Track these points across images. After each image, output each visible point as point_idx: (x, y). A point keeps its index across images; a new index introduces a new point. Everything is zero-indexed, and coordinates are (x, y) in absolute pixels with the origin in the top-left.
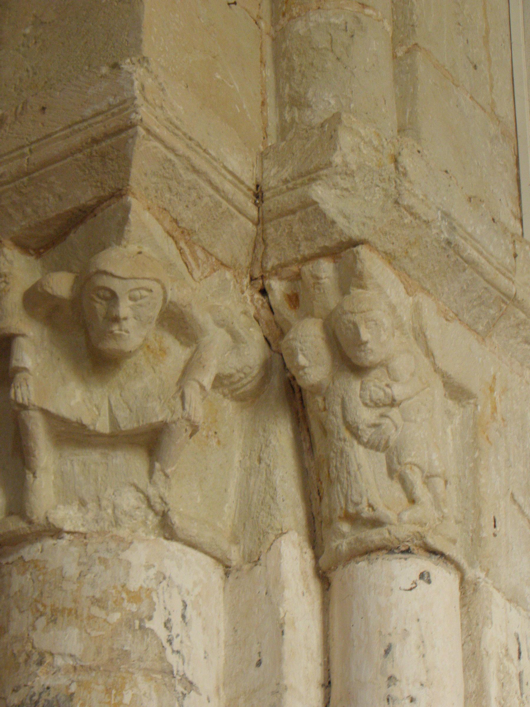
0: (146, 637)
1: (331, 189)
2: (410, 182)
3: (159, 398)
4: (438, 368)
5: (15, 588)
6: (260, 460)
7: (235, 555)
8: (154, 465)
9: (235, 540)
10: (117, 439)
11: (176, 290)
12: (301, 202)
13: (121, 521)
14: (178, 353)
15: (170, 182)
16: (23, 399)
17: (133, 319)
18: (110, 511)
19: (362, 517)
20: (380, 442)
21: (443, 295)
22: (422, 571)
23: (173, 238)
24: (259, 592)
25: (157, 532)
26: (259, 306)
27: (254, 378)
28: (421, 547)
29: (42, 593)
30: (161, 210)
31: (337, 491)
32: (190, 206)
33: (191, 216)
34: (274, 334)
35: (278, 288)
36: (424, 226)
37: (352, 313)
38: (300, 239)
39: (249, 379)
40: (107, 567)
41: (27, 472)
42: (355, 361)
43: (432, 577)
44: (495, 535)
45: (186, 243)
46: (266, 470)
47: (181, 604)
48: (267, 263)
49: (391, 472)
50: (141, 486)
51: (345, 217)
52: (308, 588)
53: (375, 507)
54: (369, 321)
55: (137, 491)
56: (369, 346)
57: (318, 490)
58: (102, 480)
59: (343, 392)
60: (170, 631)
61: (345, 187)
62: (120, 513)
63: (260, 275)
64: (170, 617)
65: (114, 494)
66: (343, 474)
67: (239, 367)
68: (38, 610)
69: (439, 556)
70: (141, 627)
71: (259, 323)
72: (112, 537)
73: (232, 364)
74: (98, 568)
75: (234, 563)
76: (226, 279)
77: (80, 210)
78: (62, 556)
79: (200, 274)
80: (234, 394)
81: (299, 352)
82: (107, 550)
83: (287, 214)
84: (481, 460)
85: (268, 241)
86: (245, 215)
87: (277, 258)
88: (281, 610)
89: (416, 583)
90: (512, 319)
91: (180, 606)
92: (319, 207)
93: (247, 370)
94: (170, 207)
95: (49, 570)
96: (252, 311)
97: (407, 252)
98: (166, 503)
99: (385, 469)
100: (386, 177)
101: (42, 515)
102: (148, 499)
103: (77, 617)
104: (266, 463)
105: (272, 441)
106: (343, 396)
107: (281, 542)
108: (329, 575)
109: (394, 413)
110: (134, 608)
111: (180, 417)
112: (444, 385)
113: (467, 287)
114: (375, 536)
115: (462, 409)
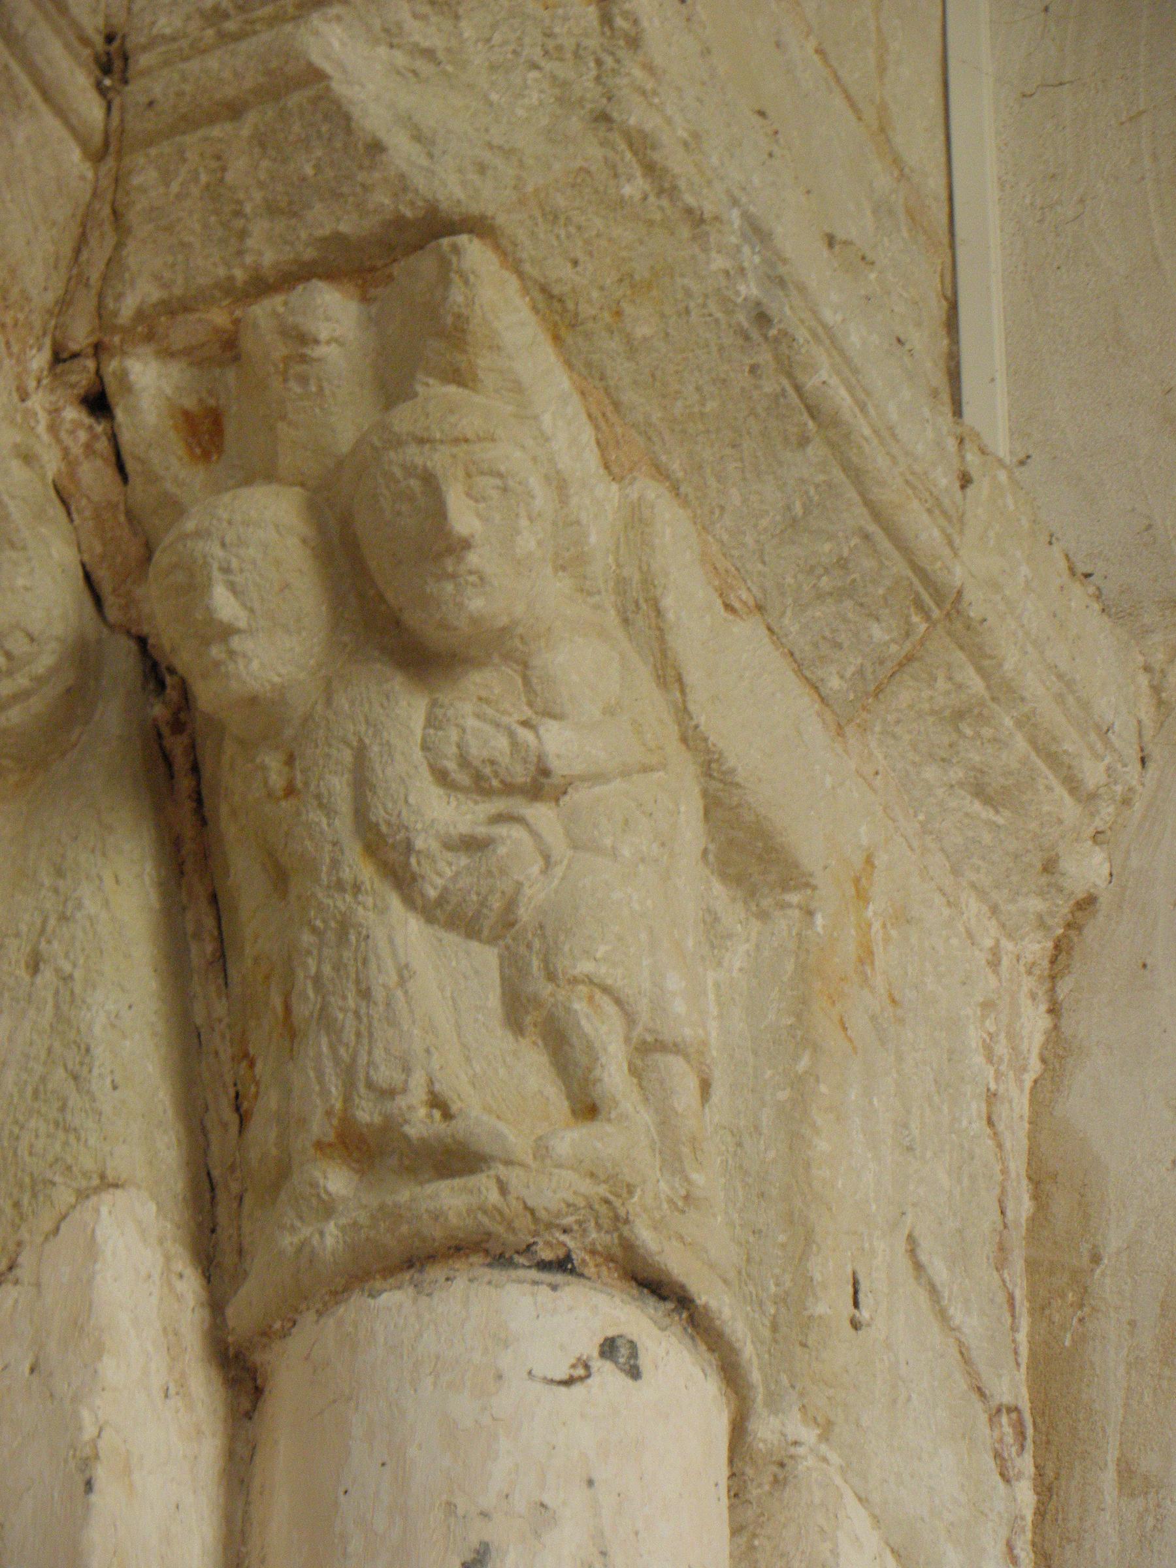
1: (377, 42)
2: (649, 68)
4: (696, 727)
6: (35, 964)
12: (269, 73)
19: (405, 1137)
20: (483, 903)
21: (721, 515)
22: (610, 1333)
26: (77, 450)
27: (39, 680)
28: (610, 1258)
31: (319, 1055)
34: (119, 560)
35: (150, 384)
36: (685, 232)
37: (421, 441)
38: (248, 208)
39: (22, 681)
42: (413, 618)
43: (644, 1361)
44: (856, 1325)
46: (57, 993)
48: (119, 297)
49: (518, 1008)
51: (418, 137)
52: (182, 1384)
53: (454, 1108)
54: (482, 473)
56: (473, 558)
57: (237, 1096)
59: (363, 728)
61: (426, 44)
63: (93, 339)
66: (344, 998)
69: (670, 1305)
71: (69, 514)
81: (216, 574)
83: (212, 119)
84: (817, 1080)
85: (133, 217)
87: (157, 278)
88: (85, 1414)
89: (587, 1367)
90: (941, 684)
92: (328, 89)
96: (52, 464)
97: (618, 314)
99: (494, 1000)
100: (569, 43)
104: (58, 970)
105: (87, 902)
106: (361, 740)
107: (97, 1211)
108: (258, 1357)
109: (541, 814)
112: (707, 812)
113: (807, 511)
114: (451, 1200)
115: (756, 925)
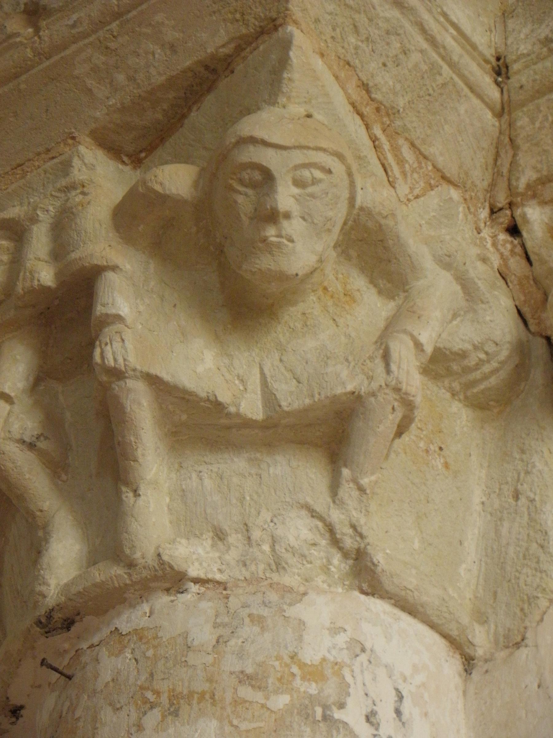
0: (335, 733)
3: (347, 360)
5: (106, 676)
6: (517, 496)
7: (481, 639)
8: (341, 471)
9: (481, 618)
10: (277, 432)
11: (371, 190)
13: (287, 563)
14: (372, 307)
15: (356, 16)
16: (115, 360)
17: (300, 220)
18: (266, 548)
23: (361, 116)
24: (526, 687)
25: (347, 583)
26: (507, 253)
27: (502, 363)
29: (152, 675)
30: (342, 63)
32: (388, 64)
33: (391, 83)
39: (494, 364)
40: (263, 629)
41: (124, 489)
45: (384, 131)
47: (394, 693)
48: (518, 179)
50: (318, 508)
55: (313, 516)
58: (252, 499)
60: (377, 729)
62: (284, 551)
63: (507, 201)
64: (375, 708)
65: (272, 521)
67: (477, 339)
68: (146, 701)
70: (325, 718)
71: (507, 283)
72: (271, 585)
73: (464, 335)
74: (248, 630)
75: (480, 652)
76: (451, 198)
77: (207, 67)
78: (187, 617)
79: (407, 191)
80: (469, 393)
82: (264, 604)
85: (519, 141)
86: (479, 96)
87: (534, 168)
91: (392, 697)
93: (490, 348)
94: (357, 61)
95: (164, 640)
96: (496, 262)
98: (361, 536)
101: (151, 552)
102: (331, 530)
103: (214, 704)
104: (528, 498)
105: (537, 464)
110: (313, 689)
111: (383, 384)
